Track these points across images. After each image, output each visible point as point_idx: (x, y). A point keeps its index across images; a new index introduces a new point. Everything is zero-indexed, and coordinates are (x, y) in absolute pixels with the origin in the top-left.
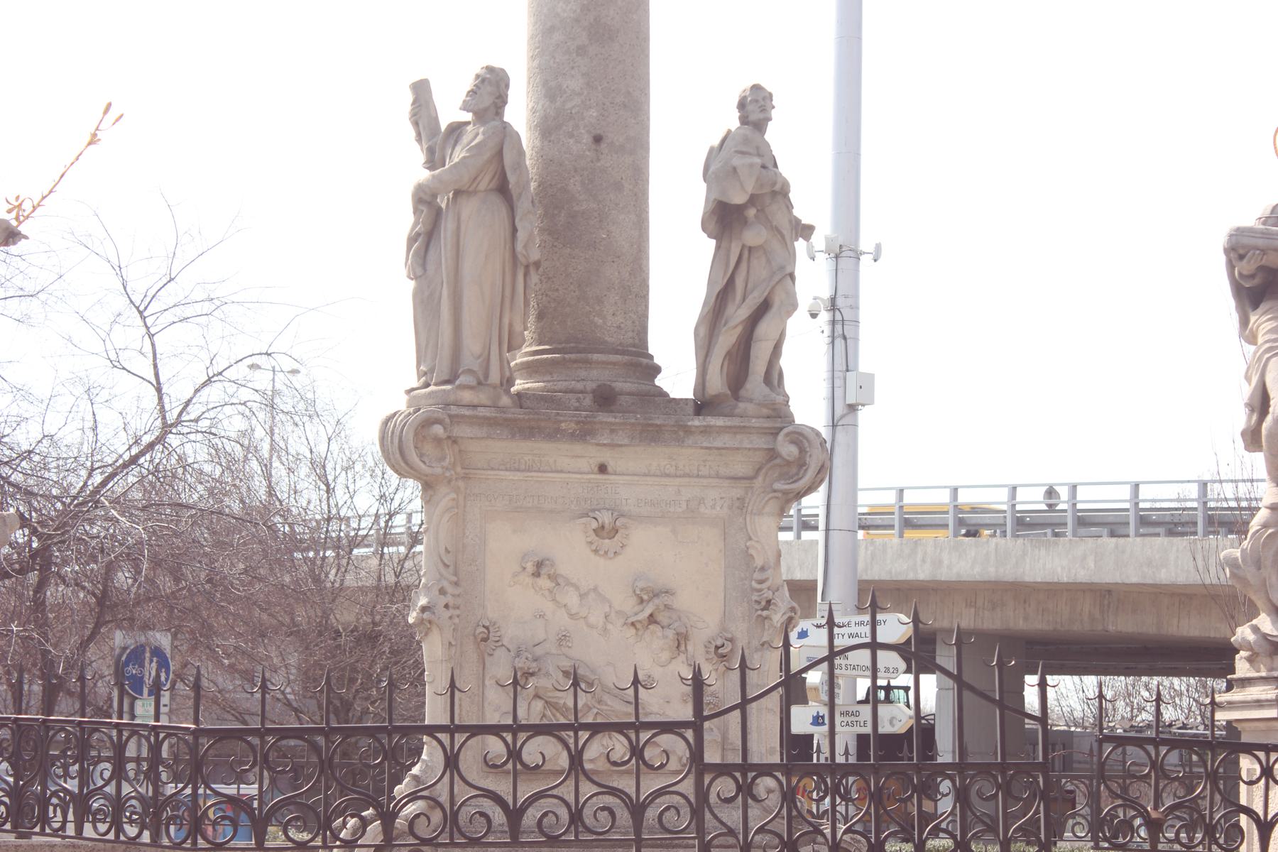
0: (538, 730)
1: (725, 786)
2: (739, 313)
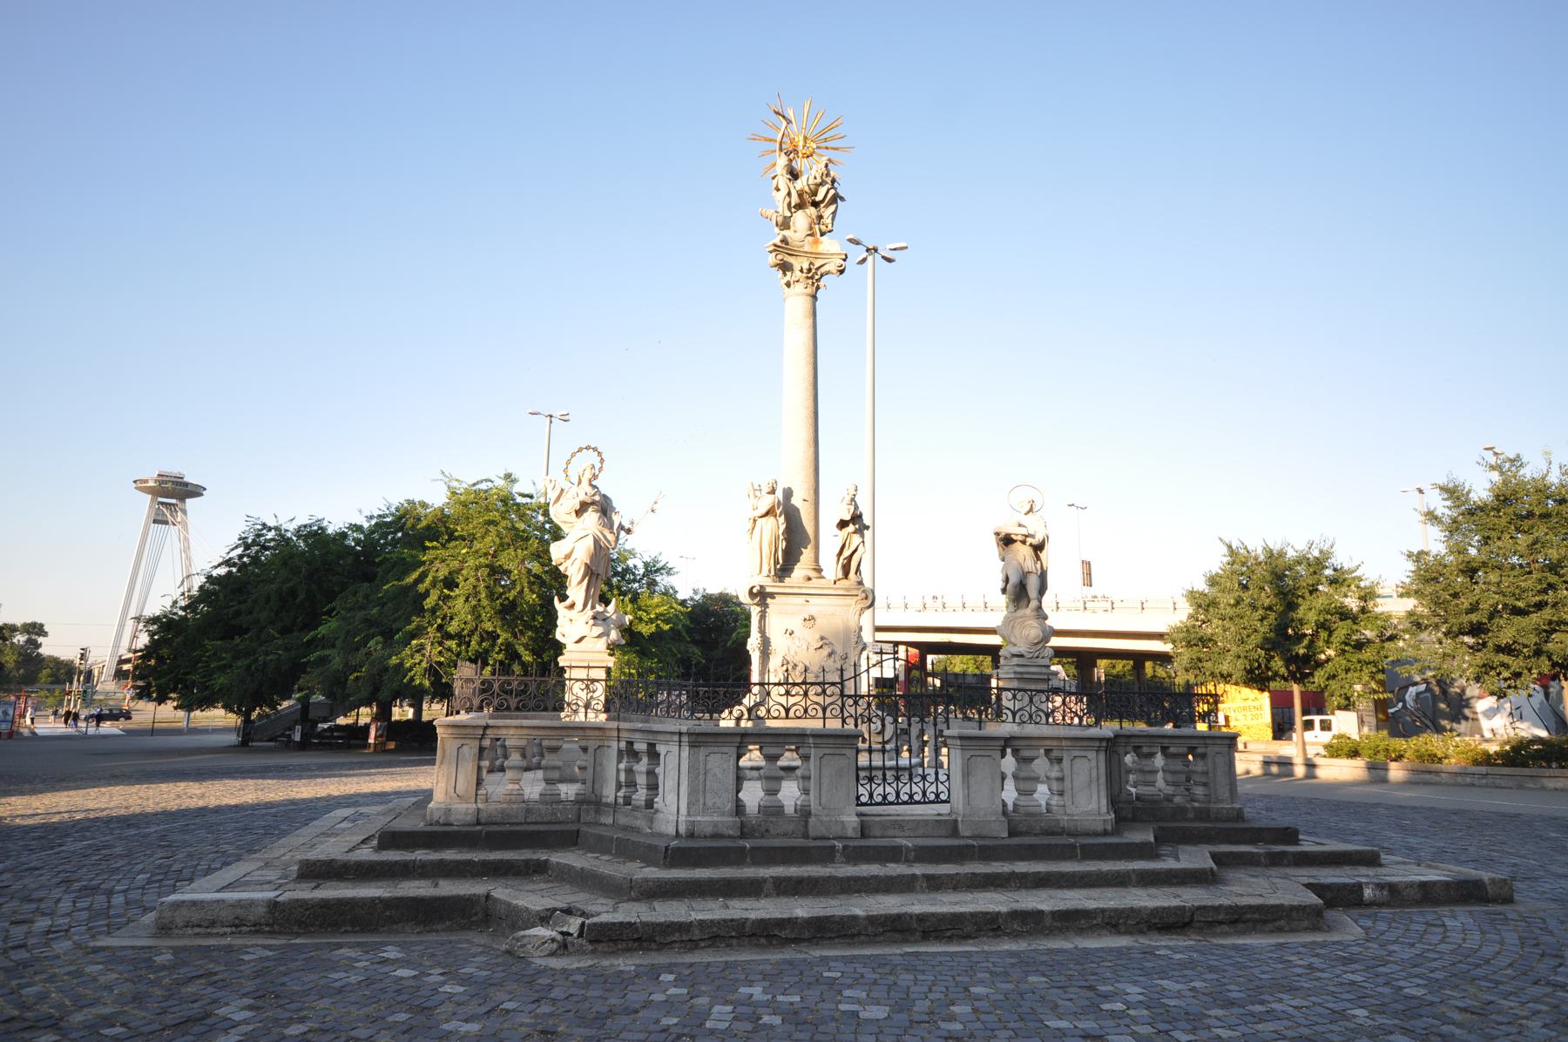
0: (794, 684)
1: (851, 701)
2: (846, 553)
